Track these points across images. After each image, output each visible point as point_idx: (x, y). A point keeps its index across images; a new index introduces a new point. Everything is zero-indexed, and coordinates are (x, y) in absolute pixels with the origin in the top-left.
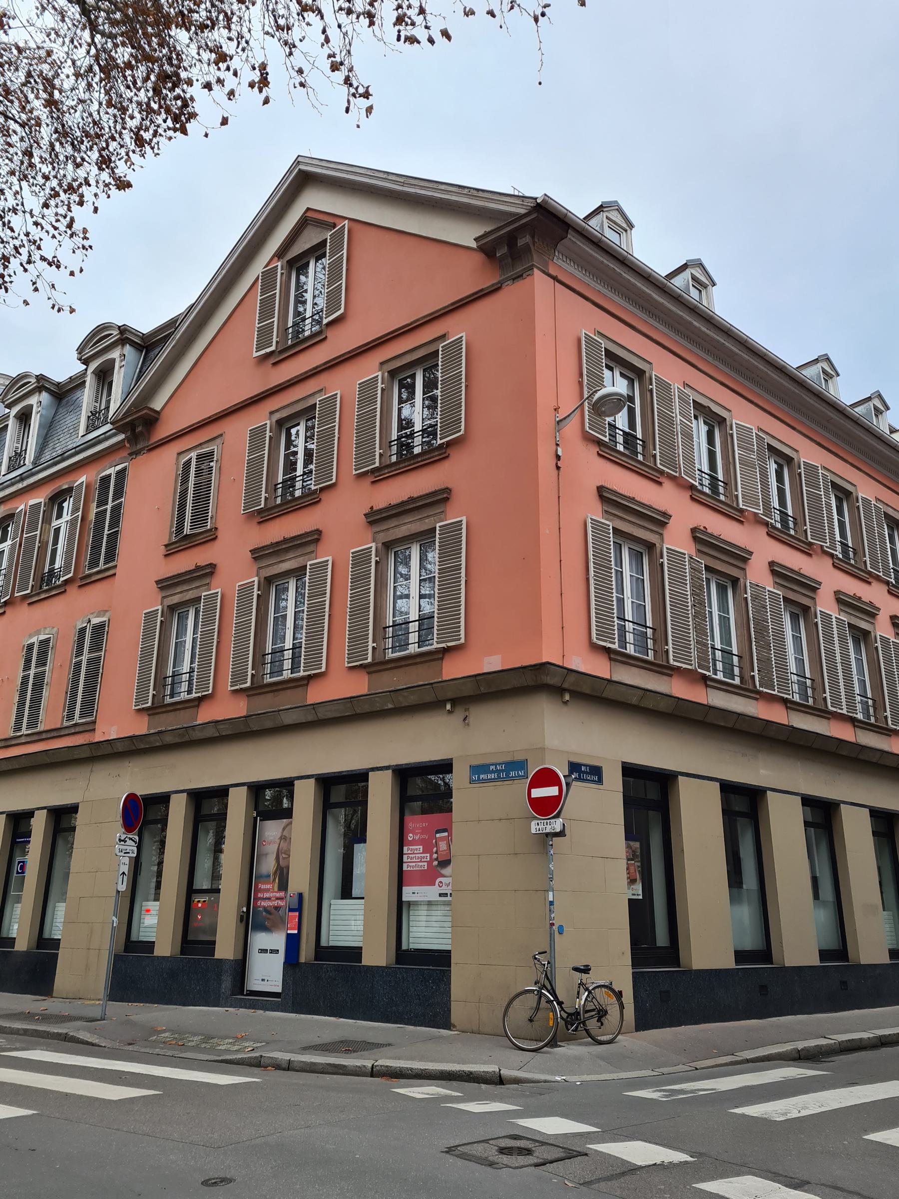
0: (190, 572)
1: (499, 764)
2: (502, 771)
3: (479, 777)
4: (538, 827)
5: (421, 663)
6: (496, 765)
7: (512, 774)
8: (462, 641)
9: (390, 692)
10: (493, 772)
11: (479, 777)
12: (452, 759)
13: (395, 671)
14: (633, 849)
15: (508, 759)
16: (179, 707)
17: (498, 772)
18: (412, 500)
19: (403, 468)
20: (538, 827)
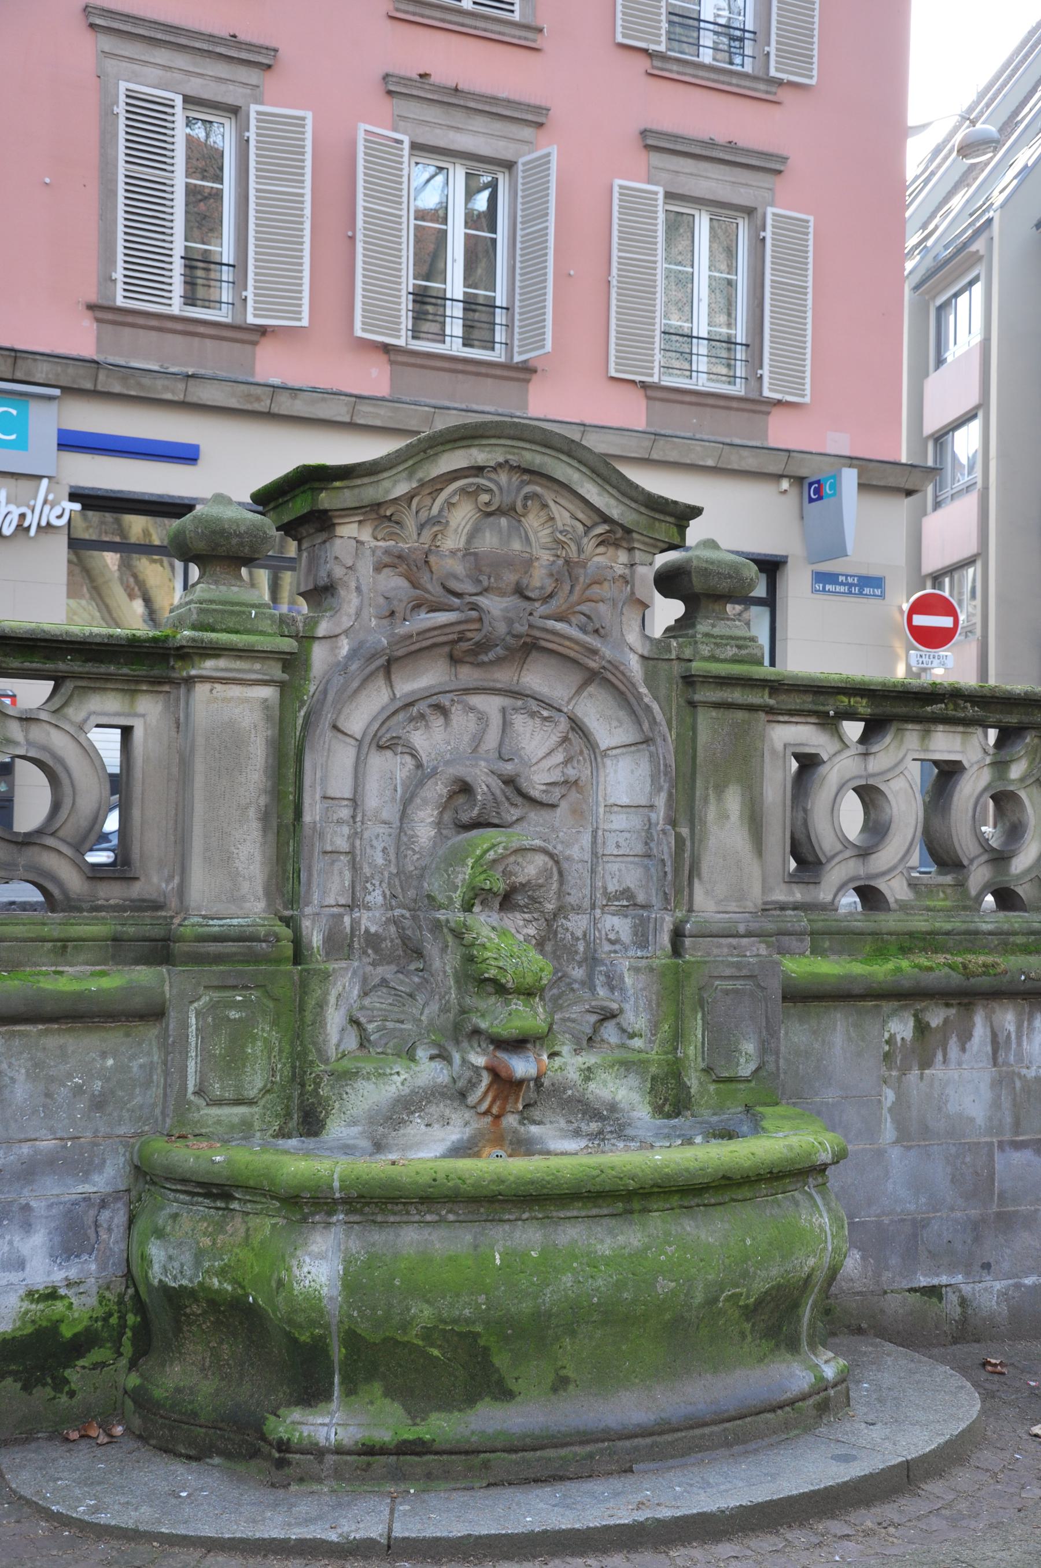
0: (211, 38)
1: (851, 576)
2: (855, 585)
3: (824, 588)
4: (921, 660)
5: (737, 410)
6: (847, 576)
7: (867, 591)
8: (549, 346)
9: (723, 444)
10: (842, 584)
11: (824, 588)
12: (787, 557)
13: (694, 408)
14: (698, 686)
15: (864, 572)
16: (201, 329)
17: (850, 585)
18: (731, 146)
19: (702, 78)
20: (921, 660)
